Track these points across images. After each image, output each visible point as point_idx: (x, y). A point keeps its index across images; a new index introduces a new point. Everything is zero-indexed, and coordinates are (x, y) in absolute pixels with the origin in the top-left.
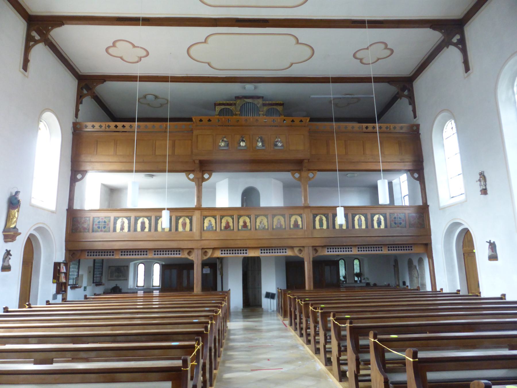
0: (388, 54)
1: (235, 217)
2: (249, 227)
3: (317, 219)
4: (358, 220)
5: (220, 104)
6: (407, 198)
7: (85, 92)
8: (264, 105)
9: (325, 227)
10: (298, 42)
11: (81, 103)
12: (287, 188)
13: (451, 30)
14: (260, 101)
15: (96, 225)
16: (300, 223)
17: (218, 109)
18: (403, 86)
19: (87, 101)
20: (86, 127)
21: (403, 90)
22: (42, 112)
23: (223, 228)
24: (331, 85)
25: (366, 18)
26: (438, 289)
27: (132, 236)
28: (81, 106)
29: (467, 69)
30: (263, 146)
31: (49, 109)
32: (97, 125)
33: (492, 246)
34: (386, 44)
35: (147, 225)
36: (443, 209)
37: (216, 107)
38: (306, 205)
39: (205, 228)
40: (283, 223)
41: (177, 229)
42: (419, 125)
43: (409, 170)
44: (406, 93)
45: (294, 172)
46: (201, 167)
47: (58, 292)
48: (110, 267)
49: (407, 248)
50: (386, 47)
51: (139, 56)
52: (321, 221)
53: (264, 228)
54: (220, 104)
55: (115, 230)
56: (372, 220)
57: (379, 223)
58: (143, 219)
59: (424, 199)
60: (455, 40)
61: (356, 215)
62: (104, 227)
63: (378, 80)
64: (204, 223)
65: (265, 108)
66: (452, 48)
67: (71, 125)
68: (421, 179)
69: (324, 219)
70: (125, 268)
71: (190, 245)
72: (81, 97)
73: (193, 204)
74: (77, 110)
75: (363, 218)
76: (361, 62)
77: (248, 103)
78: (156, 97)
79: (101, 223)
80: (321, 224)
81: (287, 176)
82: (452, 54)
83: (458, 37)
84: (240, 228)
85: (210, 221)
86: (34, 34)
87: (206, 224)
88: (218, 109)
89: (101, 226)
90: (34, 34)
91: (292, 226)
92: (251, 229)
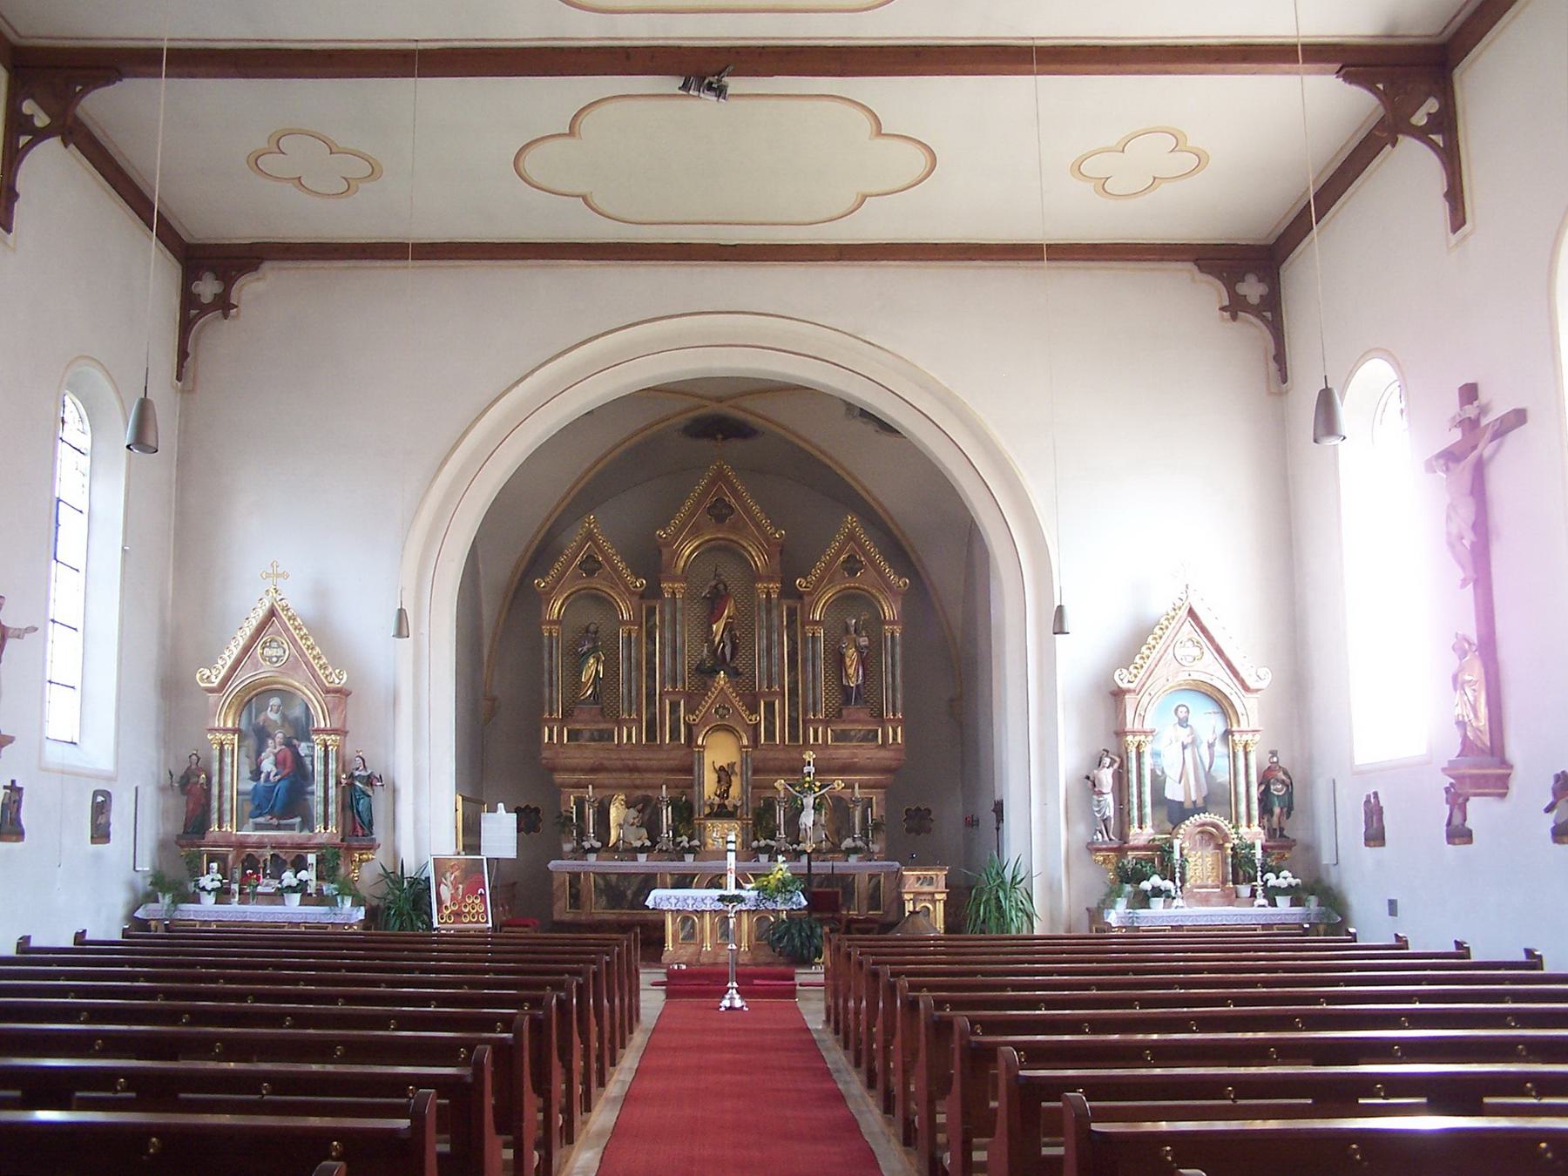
13: (1411, 82)
29: (1458, 218)
33: (101, 833)
60: (1420, 119)
66: (1409, 147)
82: (1411, 166)
83: (1432, 105)
86: (28, 107)
90: (28, 107)
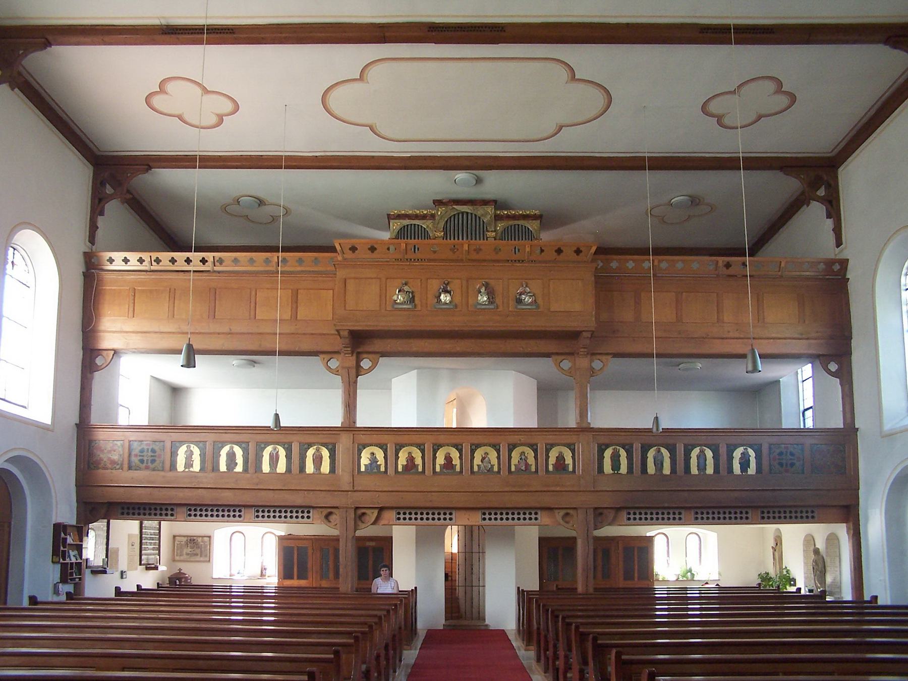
0: (784, 106)
1: (466, 449)
2: (458, 469)
3: (608, 453)
4: (698, 457)
5: (399, 217)
6: (809, 414)
7: (109, 190)
8: (498, 218)
9: (624, 469)
10: (573, 78)
11: (102, 213)
12: (546, 393)
14: (490, 210)
15: (136, 455)
16: (569, 461)
17: (396, 225)
18: (817, 176)
19: (114, 209)
20: (111, 261)
21: (814, 185)
22: (12, 230)
23: (400, 469)
24: (648, 178)
25: (731, 22)
26: (867, 597)
27: (208, 480)
28: (100, 221)
30: (491, 300)
31: (30, 224)
32: (133, 257)
34: (780, 84)
35: (240, 460)
36: (891, 436)
37: (392, 222)
38: (584, 425)
39: (363, 469)
40: (531, 460)
41: (302, 468)
42: (848, 260)
43: (818, 356)
44: (821, 192)
45: (560, 358)
46: (360, 347)
47: (64, 579)
48: (174, 537)
49: (804, 515)
50: (779, 89)
51: (219, 112)
52: (615, 458)
53: (490, 470)
54: (399, 217)
55: (173, 466)
56: (730, 458)
57: (745, 464)
58: (232, 448)
59: (848, 416)
61: (694, 446)
62: (153, 461)
63: (754, 164)
64: (360, 458)
65: (500, 226)
67: (81, 258)
68: (845, 376)
69: (623, 453)
70: (206, 539)
71: (330, 501)
72: (100, 200)
73: (335, 419)
74: (93, 228)
75: (709, 454)
76: (720, 123)
77: (463, 213)
78: (261, 202)
79: (145, 454)
80: (616, 465)
81: (545, 367)
84: (438, 469)
85: (373, 454)
87: (365, 460)
88: (396, 225)
89: (145, 458)
91: (551, 468)
92: (461, 472)
